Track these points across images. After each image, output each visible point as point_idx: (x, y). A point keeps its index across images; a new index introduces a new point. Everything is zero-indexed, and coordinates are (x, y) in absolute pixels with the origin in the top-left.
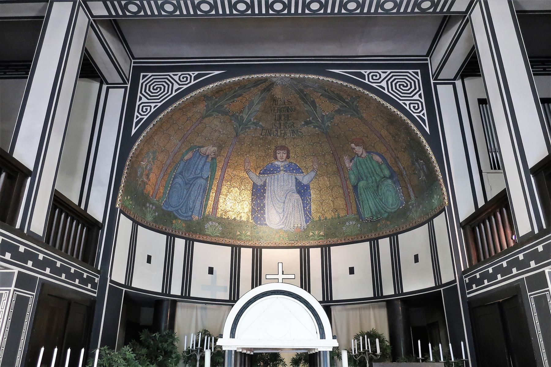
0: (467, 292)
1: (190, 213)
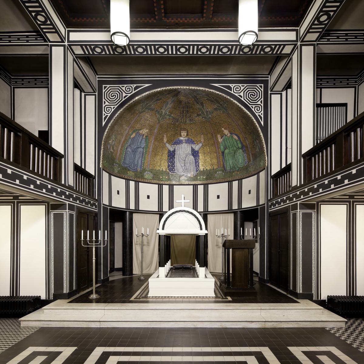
1: (136, 167)
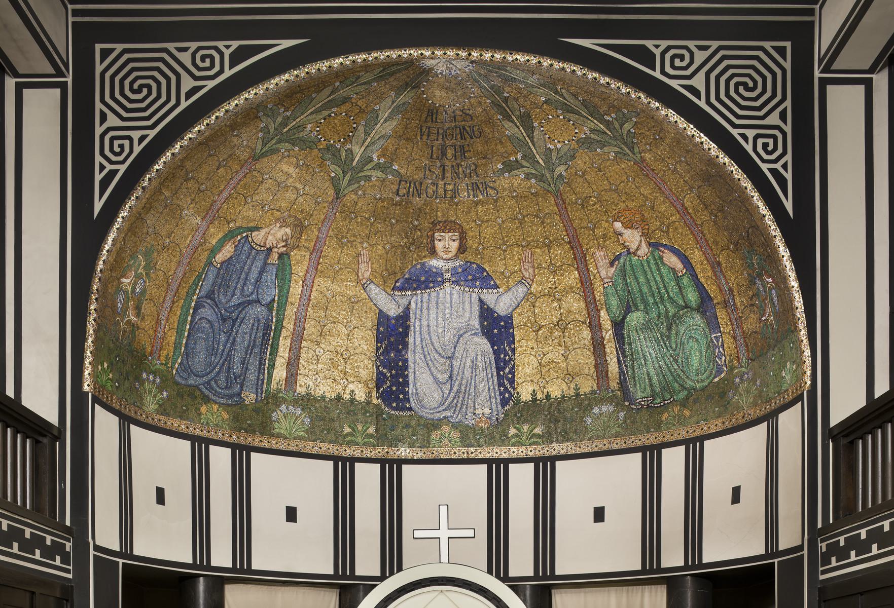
0: (821, 569)
1: (237, 388)
